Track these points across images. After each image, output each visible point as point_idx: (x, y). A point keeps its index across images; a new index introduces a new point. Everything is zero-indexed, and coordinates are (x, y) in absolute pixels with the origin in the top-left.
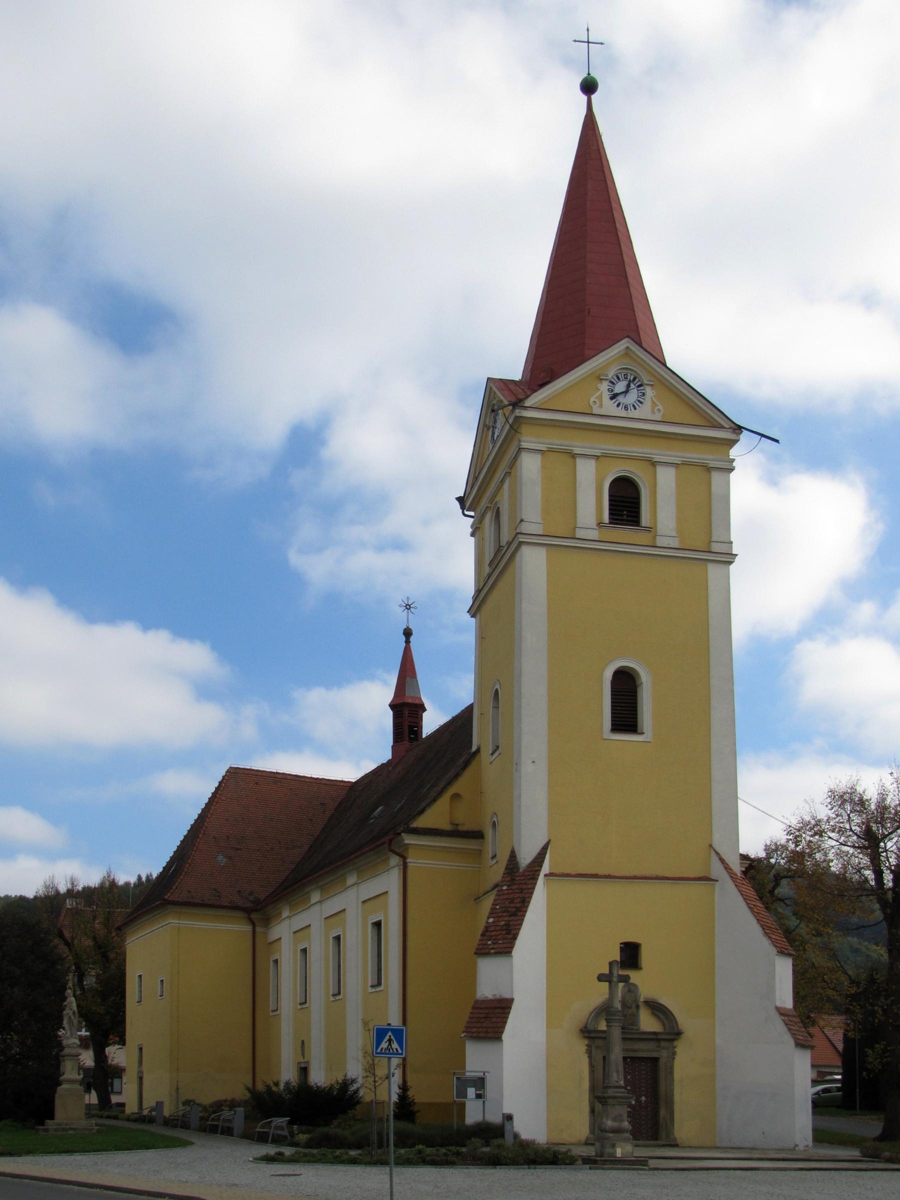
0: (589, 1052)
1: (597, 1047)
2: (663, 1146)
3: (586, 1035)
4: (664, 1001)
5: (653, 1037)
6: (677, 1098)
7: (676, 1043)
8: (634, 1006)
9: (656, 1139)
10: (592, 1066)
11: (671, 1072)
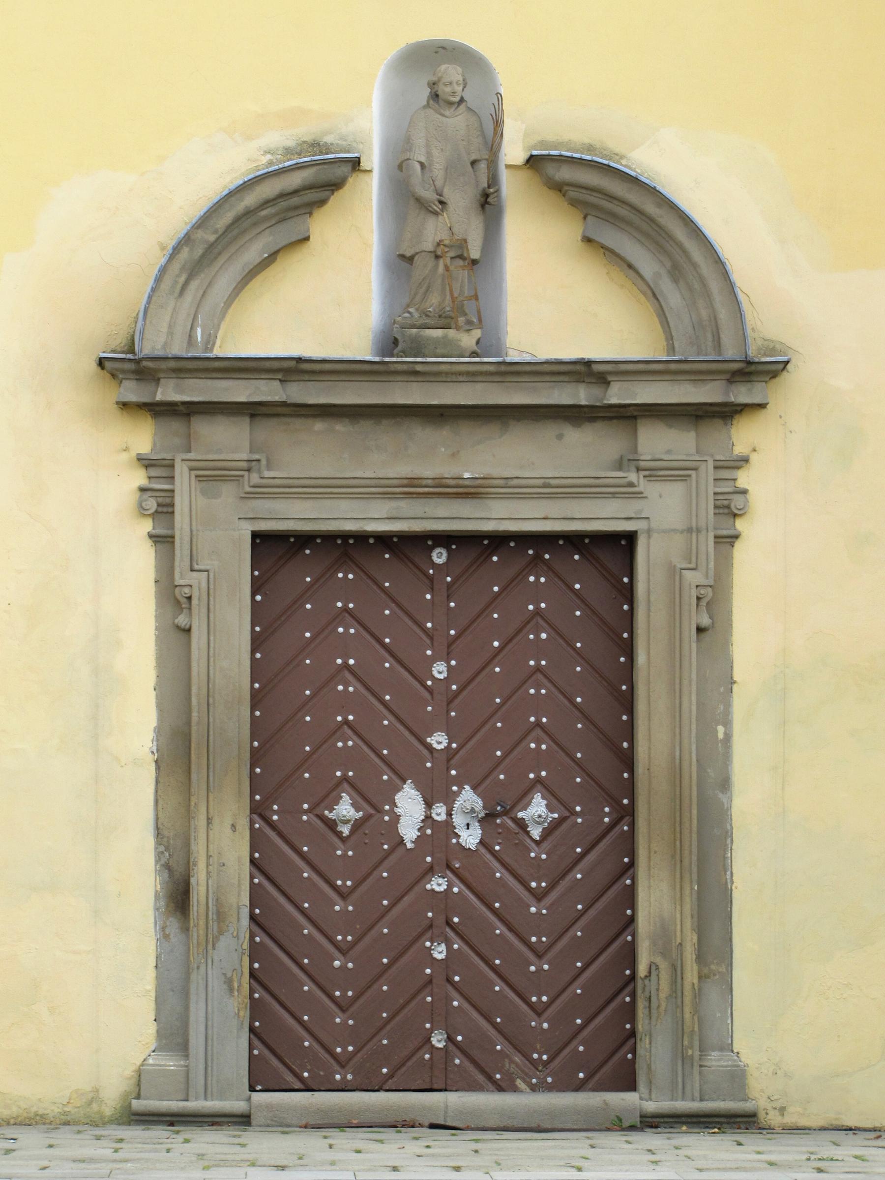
0: (160, 507)
1: (211, 476)
2: (651, 1122)
3: (132, 392)
4: (672, 161)
5: (582, 395)
6: (749, 801)
7: (744, 435)
8: (461, 200)
9: (627, 1081)
10: (173, 599)
11: (710, 628)
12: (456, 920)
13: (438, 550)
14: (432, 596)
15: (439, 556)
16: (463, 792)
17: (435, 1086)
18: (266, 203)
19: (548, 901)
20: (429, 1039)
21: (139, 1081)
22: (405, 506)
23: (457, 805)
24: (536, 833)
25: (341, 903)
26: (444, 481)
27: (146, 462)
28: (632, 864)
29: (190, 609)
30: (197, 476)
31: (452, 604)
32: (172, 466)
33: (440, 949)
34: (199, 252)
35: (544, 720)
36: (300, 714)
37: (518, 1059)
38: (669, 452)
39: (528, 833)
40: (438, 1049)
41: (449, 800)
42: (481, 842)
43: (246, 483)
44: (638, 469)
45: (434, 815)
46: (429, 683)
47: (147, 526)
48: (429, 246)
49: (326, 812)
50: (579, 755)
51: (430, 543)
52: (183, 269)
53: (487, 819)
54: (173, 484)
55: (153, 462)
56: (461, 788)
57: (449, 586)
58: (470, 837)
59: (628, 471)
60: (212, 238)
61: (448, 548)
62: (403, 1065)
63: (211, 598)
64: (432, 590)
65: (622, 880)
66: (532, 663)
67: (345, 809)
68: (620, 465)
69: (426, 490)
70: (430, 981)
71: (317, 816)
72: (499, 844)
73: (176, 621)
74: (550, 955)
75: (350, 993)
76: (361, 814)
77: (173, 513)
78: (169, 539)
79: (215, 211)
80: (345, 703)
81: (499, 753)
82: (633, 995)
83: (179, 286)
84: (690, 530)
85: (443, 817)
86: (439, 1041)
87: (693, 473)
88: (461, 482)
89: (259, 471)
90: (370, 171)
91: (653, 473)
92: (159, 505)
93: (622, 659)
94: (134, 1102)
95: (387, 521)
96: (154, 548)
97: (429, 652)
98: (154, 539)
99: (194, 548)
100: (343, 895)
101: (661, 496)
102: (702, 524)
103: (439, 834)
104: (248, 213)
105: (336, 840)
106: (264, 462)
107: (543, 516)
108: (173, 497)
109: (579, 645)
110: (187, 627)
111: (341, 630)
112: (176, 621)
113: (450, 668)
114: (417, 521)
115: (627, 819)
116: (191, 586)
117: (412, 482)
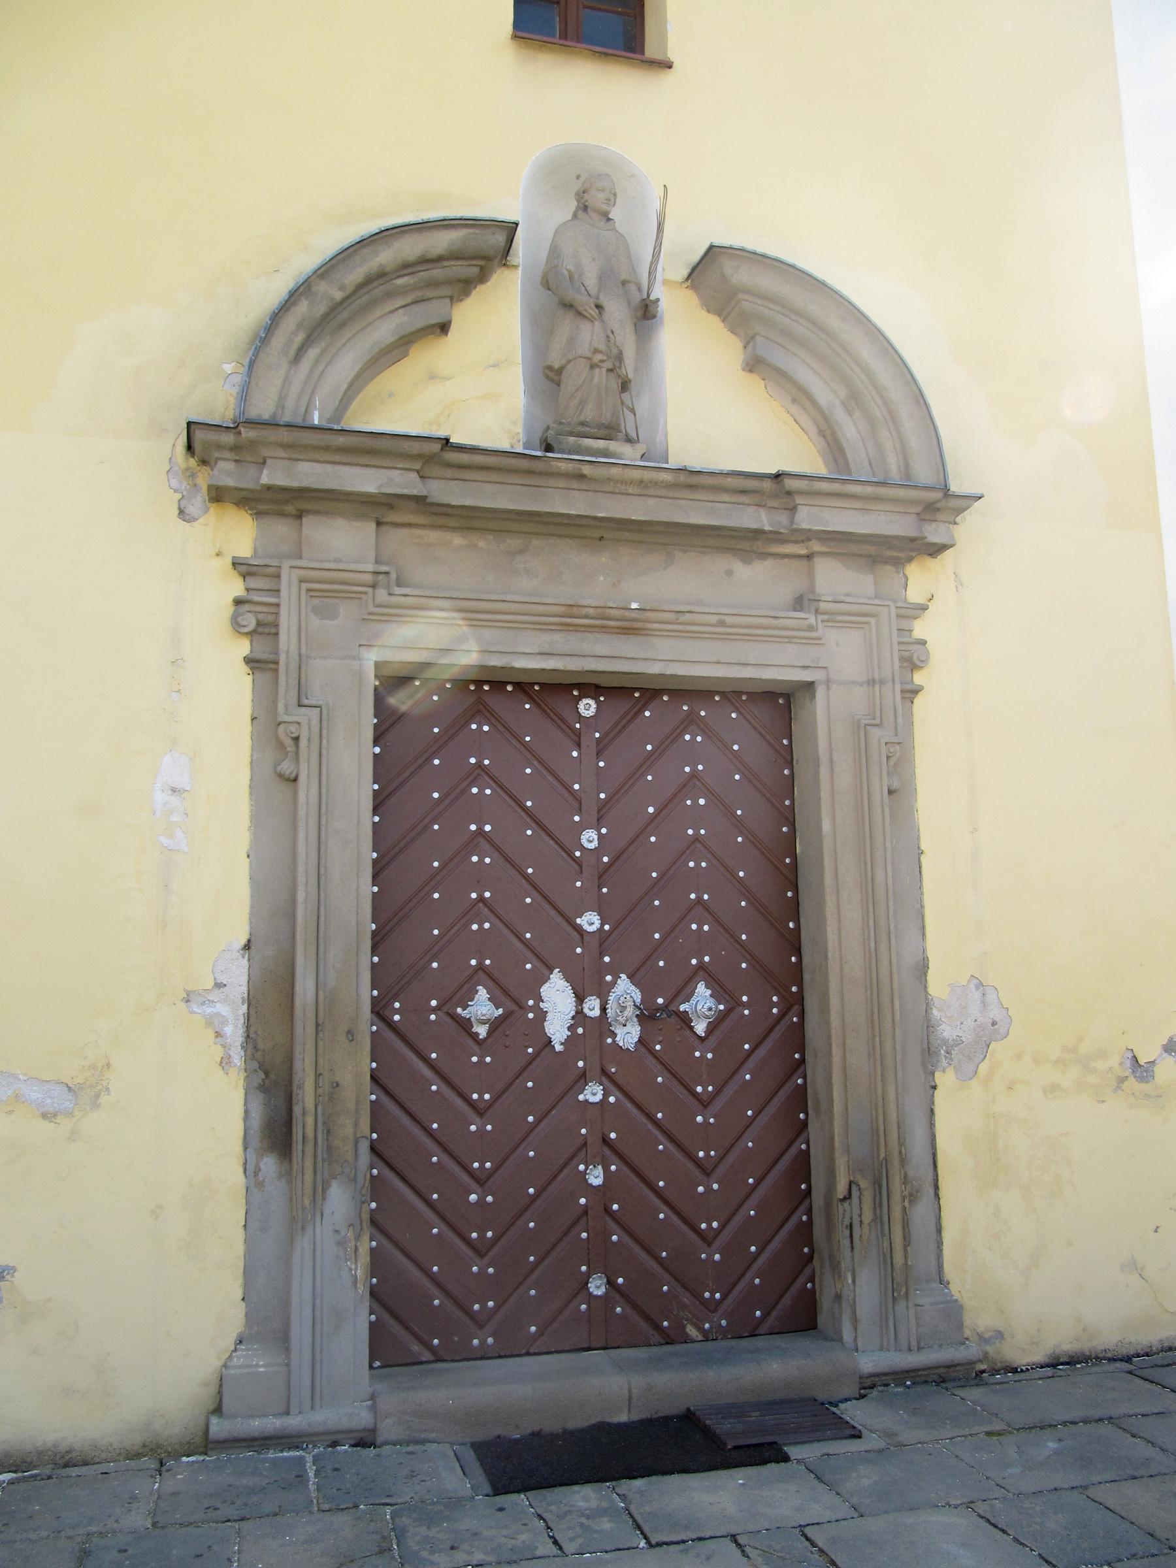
3: (226, 473)
7: (920, 579)
8: (618, 313)
12: (613, 1135)
13: (585, 701)
14: (580, 754)
15: (587, 707)
16: (619, 981)
17: (593, 1345)
18: (406, 267)
19: (717, 1105)
20: (587, 1283)
21: (221, 1386)
22: (559, 641)
23: (612, 997)
24: (700, 1028)
25: (478, 1120)
26: (607, 610)
27: (243, 569)
28: (803, 1060)
29: (297, 753)
30: (308, 590)
31: (602, 764)
32: (278, 576)
33: (596, 1172)
34: (321, 309)
35: (706, 897)
36: (533, 824)
37: (686, 1299)
38: (847, 595)
39: (692, 1028)
40: (596, 1297)
41: (603, 992)
42: (640, 1041)
43: (370, 601)
44: (817, 612)
45: (586, 1011)
46: (578, 854)
47: (244, 647)
48: (585, 350)
49: (459, 1010)
50: (744, 937)
51: (575, 693)
52: (300, 326)
53: (647, 1016)
54: (278, 597)
55: (255, 569)
56: (616, 978)
57: (598, 741)
58: (628, 1035)
59: (809, 612)
60: (338, 295)
61: (596, 699)
62: (554, 1320)
63: (324, 741)
64: (578, 746)
65: (793, 1079)
66: (690, 832)
67: (482, 1007)
68: (799, 603)
69: (586, 621)
70: (585, 1211)
71: (448, 1014)
72: (660, 1043)
73: (279, 768)
74: (720, 1172)
75: (490, 1234)
76: (501, 1011)
77: (277, 634)
78: (271, 666)
79: (344, 260)
80: (480, 878)
81: (657, 936)
82: (809, 1212)
83: (295, 347)
84: (871, 682)
85: (596, 1013)
86: (598, 1287)
87: (872, 621)
88: (627, 614)
89: (388, 587)
90: (516, 267)
91: (831, 619)
92: (259, 624)
93: (785, 829)
94: (214, 1420)
95: (539, 657)
96: (250, 677)
97: (577, 818)
98: (253, 665)
99: (303, 679)
100: (480, 1110)
101: (838, 645)
102: (887, 674)
103: (592, 1032)
104: (381, 275)
105: (471, 1043)
106: (393, 575)
107: (715, 659)
108: (277, 614)
109: (739, 812)
110: (293, 775)
111: (475, 790)
112: (279, 768)
113: (600, 835)
114: (574, 658)
115: (796, 1008)
116: (299, 723)
117: (572, 610)
